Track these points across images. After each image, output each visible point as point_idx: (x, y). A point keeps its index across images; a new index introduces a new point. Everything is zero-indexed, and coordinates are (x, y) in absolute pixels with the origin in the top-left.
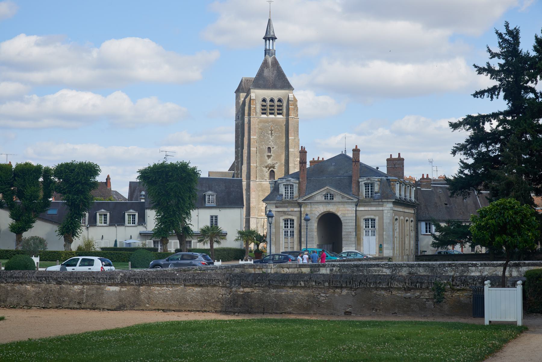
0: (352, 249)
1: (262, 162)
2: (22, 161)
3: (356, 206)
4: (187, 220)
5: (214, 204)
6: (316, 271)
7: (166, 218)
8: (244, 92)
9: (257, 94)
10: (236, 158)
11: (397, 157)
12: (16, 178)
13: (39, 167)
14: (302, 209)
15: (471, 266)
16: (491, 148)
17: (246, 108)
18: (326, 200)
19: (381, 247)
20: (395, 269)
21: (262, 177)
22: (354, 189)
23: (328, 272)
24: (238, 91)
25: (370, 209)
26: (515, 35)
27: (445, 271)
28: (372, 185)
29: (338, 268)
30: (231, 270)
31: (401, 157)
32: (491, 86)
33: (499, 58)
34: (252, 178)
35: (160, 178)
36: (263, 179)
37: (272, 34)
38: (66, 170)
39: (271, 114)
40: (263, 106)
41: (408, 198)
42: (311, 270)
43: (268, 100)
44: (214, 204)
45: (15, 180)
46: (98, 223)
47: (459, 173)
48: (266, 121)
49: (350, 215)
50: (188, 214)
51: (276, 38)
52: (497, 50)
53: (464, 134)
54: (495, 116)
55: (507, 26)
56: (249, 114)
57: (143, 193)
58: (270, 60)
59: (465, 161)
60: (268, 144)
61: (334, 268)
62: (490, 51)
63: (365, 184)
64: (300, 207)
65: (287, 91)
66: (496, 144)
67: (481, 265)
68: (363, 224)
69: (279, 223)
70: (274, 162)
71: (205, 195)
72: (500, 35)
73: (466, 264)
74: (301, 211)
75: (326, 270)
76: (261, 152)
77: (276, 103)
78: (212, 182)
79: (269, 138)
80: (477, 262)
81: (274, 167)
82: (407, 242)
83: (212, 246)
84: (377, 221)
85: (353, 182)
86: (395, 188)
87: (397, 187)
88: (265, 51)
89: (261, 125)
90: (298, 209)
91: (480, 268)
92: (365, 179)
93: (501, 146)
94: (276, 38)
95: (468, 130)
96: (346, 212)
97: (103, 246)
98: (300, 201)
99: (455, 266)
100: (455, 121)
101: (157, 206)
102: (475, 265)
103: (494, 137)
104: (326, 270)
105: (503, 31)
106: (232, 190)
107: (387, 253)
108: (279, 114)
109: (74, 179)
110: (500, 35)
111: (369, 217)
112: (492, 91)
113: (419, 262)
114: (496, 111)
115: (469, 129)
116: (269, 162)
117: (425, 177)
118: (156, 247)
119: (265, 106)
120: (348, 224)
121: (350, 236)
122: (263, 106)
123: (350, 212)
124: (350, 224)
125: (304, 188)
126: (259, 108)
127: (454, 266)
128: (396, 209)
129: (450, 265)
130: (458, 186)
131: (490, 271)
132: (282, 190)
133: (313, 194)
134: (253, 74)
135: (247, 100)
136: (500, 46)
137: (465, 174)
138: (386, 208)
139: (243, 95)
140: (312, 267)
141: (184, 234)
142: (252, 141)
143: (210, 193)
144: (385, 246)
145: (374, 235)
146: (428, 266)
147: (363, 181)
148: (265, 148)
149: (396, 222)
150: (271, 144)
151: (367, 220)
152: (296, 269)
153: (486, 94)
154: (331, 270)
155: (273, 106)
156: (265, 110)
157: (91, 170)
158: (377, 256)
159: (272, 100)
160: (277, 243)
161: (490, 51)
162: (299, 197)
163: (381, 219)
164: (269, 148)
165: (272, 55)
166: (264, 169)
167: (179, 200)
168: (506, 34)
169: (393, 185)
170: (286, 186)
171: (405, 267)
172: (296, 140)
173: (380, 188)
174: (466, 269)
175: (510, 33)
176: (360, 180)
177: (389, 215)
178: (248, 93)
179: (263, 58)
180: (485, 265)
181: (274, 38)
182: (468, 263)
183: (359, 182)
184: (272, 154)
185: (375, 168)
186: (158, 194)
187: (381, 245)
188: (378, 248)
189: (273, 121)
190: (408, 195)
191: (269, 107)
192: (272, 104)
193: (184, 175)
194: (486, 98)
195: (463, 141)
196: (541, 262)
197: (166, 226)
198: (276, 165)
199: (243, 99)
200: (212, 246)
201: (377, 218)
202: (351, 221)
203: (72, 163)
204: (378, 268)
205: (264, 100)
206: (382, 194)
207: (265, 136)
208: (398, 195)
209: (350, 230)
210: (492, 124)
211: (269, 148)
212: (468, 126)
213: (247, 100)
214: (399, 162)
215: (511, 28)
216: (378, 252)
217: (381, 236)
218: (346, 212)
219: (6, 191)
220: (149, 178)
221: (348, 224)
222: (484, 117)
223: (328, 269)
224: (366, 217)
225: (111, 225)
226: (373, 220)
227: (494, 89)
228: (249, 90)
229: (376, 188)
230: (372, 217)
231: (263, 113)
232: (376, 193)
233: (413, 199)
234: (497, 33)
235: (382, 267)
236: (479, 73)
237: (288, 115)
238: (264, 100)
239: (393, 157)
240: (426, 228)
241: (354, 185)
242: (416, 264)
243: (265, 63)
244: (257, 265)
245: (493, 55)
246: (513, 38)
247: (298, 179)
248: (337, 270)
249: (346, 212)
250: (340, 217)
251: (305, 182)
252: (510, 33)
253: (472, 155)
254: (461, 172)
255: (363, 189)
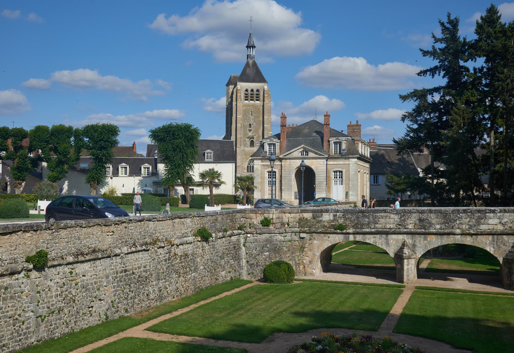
0: (324, 195)
1: (245, 134)
2: (57, 123)
3: (327, 160)
4: (190, 172)
5: (212, 160)
6: (319, 217)
7: (172, 169)
8: (232, 85)
9: (242, 86)
10: (227, 132)
11: (355, 123)
12: (53, 138)
13: (70, 128)
14: (283, 163)
15: (489, 213)
16: (432, 115)
17: (234, 96)
18: (302, 156)
19: (347, 194)
20: (404, 215)
21: (245, 145)
22: (325, 147)
23: (332, 218)
24: (228, 85)
25: (335, 163)
26: (454, 24)
27: (459, 218)
28: (340, 143)
29: (342, 214)
30: (232, 215)
31: (359, 123)
32: (433, 66)
33: (441, 43)
34: (238, 145)
35: (167, 136)
36: (245, 146)
37: (252, 43)
38: (91, 131)
39: (251, 100)
40: (246, 94)
41: (366, 155)
42: (313, 215)
43: (249, 90)
44: (212, 160)
45: (51, 138)
46: (120, 174)
47: (406, 136)
48: (248, 105)
49: (322, 168)
50: (191, 167)
51: (255, 47)
52: (439, 34)
53: (411, 105)
54: (437, 90)
55: (449, 17)
56: (236, 101)
57: (156, 151)
58: (251, 62)
59: (411, 126)
60: (249, 122)
61: (338, 214)
62: (434, 37)
63: (334, 143)
64: (281, 161)
65: (263, 84)
66: (435, 113)
67: (501, 211)
68: (332, 175)
69: (264, 174)
70: (254, 134)
71: (204, 153)
72: (442, 24)
73: (483, 211)
74: (281, 165)
75: (329, 215)
76: (244, 127)
77: (255, 92)
78: (209, 144)
79: (250, 118)
80: (496, 208)
81: (253, 138)
82: (365, 191)
83: (211, 191)
84: (344, 173)
85: (325, 141)
86: (358, 146)
87: (360, 144)
88: (248, 56)
89: (244, 108)
90: (280, 163)
91: (499, 214)
92: (334, 139)
93: (439, 115)
94: (255, 47)
95: (415, 101)
96: (319, 165)
97: (124, 192)
98: (281, 156)
99: (471, 212)
100: (404, 94)
101: (166, 160)
102: (493, 212)
103: (434, 107)
104: (329, 215)
105: (445, 20)
106: (225, 149)
107: (352, 199)
108: (257, 100)
109: (98, 137)
110: (442, 24)
111: (337, 169)
112: (433, 71)
113: (458, 208)
114: (437, 86)
115: (417, 100)
116: (250, 134)
117: (372, 141)
118: (166, 193)
119: (247, 94)
120: (320, 175)
121: (322, 185)
122: (246, 94)
123: (322, 165)
124: (322, 175)
125: (285, 146)
126: (243, 95)
127: (469, 212)
128: (359, 163)
129: (465, 211)
130: (404, 146)
131: (511, 218)
132: (267, 148)
133: (291, 151)
134: (238, 73)
135: (235, 90)
136: (443, 33)
137: (411, 137)
138: (351, 163)
139: (231, 87)
140: (315, 212)
141: (188, 182)
142: (238, 119)
143: (209, 151)
144: (350, 193)
145: (342, 184)
146: (440, 212)
147: (333, 140)
148: (247, 124)
149: (359, 173)
150: (252, 122)
151: (335, 172)
152: (298, 214)
153: (428, 73)
154: (335, 216)
155: (253, 94)
156: (247, 97)
157: (111, 131)
158: (344, 201)
159: (252, 90)
160: (262, 191)
161: (434, 37)
162: (280, 154)
163: (348, 171)
164: (250, 125)
165: (252, 58)
166: (247, 139)
167: (183, 155)
168: (448, 23)
169: (357, 143)
170: (270, 145)
171: (415, 213)
172: (269, 119)
173: (347, 146)
174: (482, 216)
175: (450, 22)
176: (330, 140)
177: (354, 168)
178: (236, 85)
179: (246, 61)
180: (505, 211)
181: (254, 47)
182: (486, 210)
183: (329, 141)
184: (252, 128)
185: (340, 131)
186: (166, 150)
187: (347, 192)
188: (344, 195)
189: (253, 105)
190: (366, 152)
191: (251, 95)
192: (252, 93)
193: (187, 134)
194: (428, 75)
195: (410, 110)
196: (512, 208)
197: (172, 176)
198: (255, 137)
199: (231, 90)
200: (211, 191)
201: (344, 171)
202: (322, 173)
203: (96, 125)
204: (385, 214)
205: (247, 90)
206: (348, 150)
207: (247, 116)
208: (360, 152)
209: (322, 180)
210: (433, 97)
211: (250, 125)
212: (415, 98)
213: (235, 90)
214: (357, 127)
215: (452, 18)
216: (345, 197)
217: (348, 185)
218: (319, 165)
219: (43, 148)
220: (159, 136)
221: (320, 175)
222: (429, 90)
223: (332, 214)
224: (335, 170)
225: (129, 176)
226: (341, 172)
227: (436, 68)
228: (236, 83)
229: (344, 146)
230: (340, 169)
231: (246, 100)
232: (343, 150)
233: (369, 156)
234: (440, 22)
235: (390, 213)
236: (424, 56)
237: (264, 101)
238: (247, 90)
239: (352, 124)
240: (374, 180)
241: (325, 144)
242: (427, 210)
243: (247, 64)
244: (259, 211)
245: (437, 40)
246: (453, 27)
247: (279, 139)
248: (341, 216)
249: (318, 165)
250: (314, 169)
251: (286, 141)
252: (450, 22)
253: (416, 122)
254: (408, 135)
255: (333, 146)
